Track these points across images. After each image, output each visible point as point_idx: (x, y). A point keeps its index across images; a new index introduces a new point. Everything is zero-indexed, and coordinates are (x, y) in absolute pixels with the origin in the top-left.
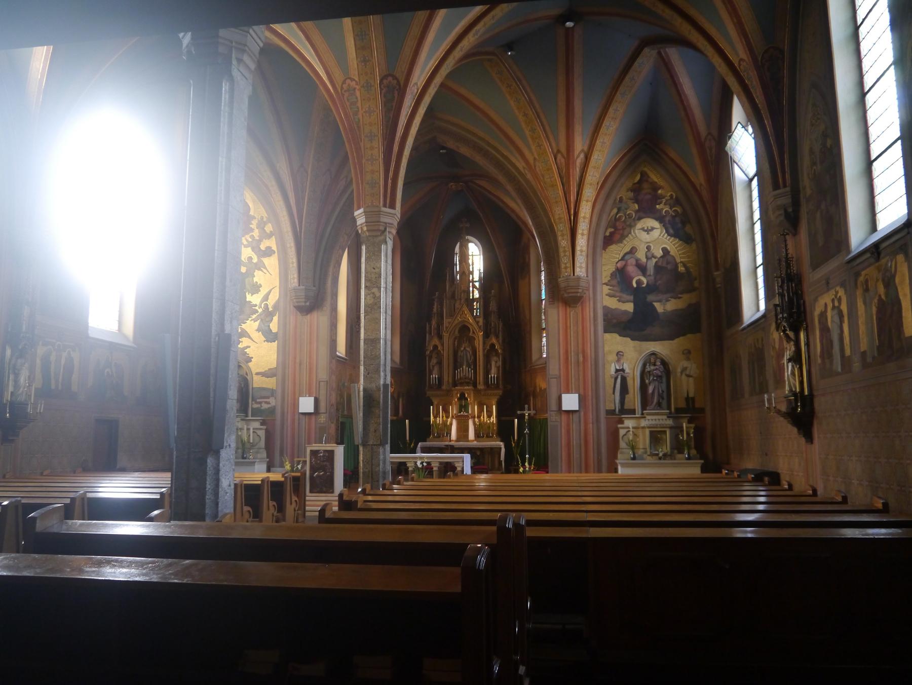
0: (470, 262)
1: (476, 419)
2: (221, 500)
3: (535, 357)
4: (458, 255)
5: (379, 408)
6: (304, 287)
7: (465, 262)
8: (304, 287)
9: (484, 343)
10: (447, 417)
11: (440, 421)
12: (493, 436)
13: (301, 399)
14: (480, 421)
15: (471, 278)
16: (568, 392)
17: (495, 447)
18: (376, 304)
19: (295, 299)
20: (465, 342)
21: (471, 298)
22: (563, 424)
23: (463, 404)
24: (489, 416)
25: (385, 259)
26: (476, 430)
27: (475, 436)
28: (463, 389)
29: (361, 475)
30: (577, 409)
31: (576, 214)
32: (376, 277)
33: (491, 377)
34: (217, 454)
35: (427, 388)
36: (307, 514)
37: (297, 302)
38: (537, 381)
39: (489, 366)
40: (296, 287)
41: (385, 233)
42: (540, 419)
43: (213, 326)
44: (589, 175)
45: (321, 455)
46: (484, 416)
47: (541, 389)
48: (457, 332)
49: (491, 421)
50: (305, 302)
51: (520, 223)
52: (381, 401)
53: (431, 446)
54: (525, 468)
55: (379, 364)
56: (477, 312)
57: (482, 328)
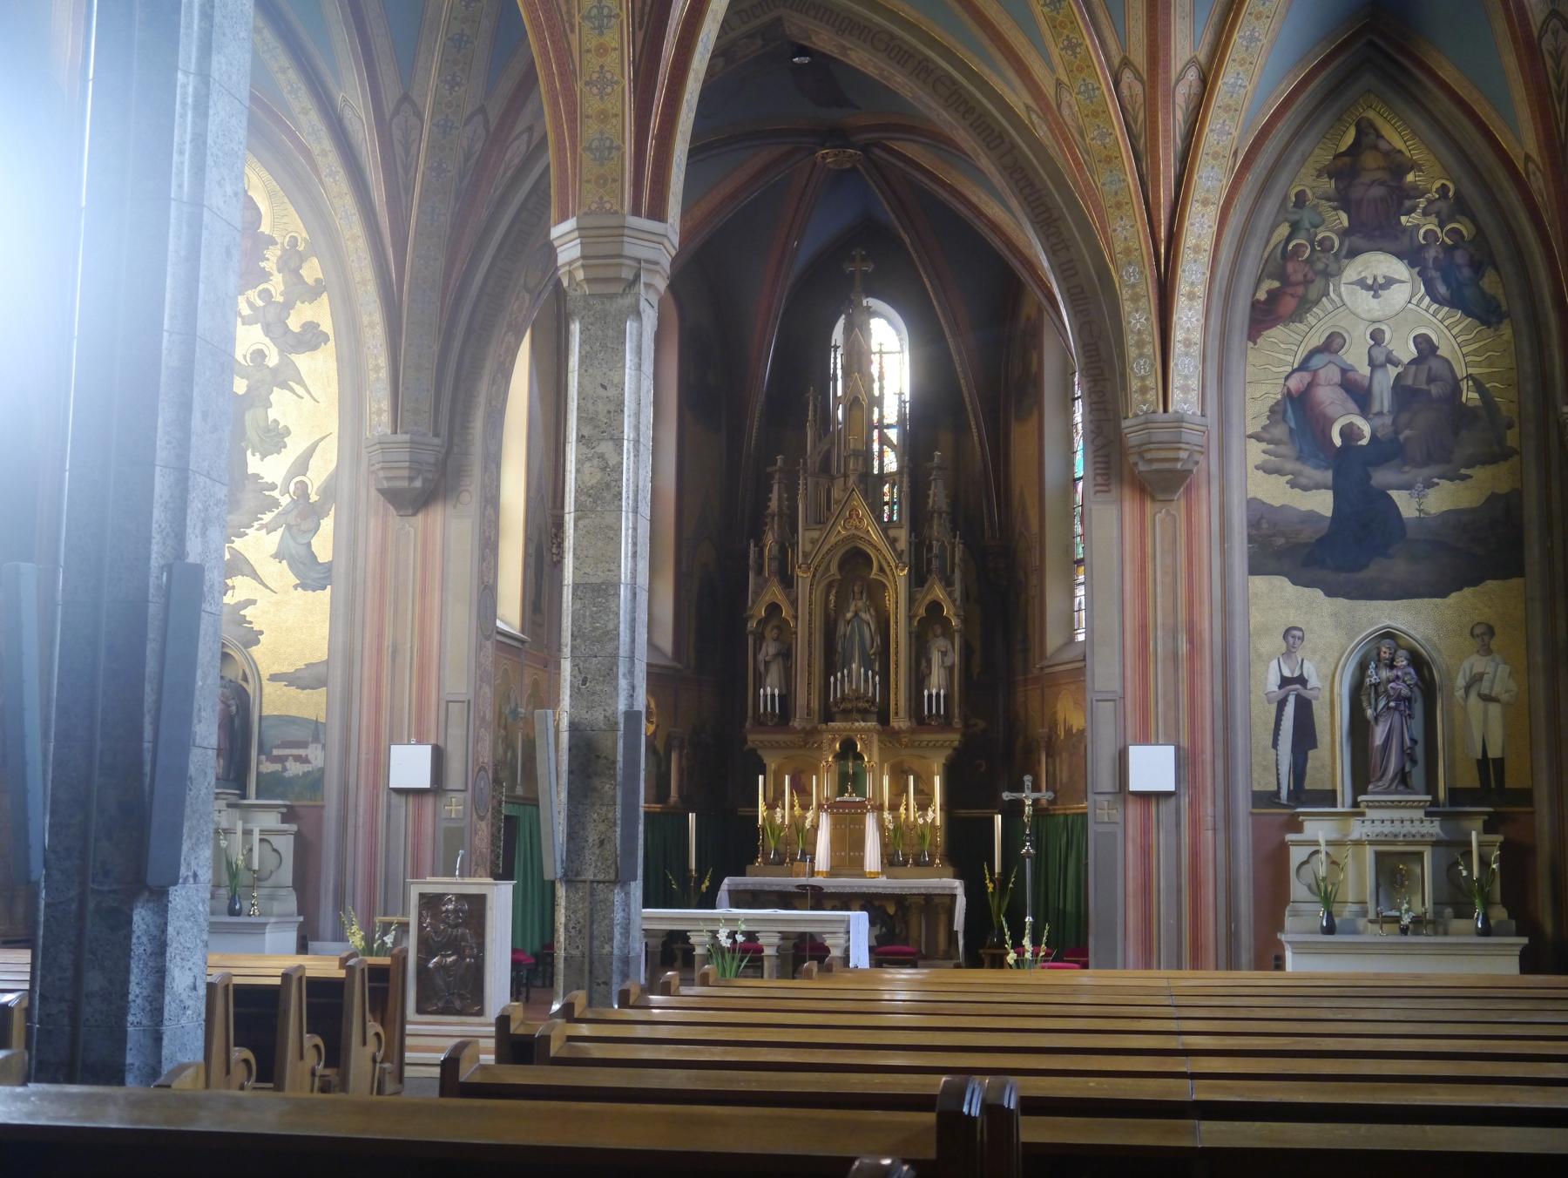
0: (875, 370)
2: (168, 1029)
3: (1053, 640)
4: (840, 352)
5: (614, 777)
6: (407, 437)
8: (407, 437)
9: (911, 600)
10: (805, 807)
11: (783, 817)
12: (930, 864)
13: (396, 750)
14: (896, 818)
15: (876, 417)
16: (1145, 739)
18: (608, 486)
19: (382, 468)
20: (857, 596)
22: (1130, 831)
23: (851, 772)
24: (923, 806)
25: (637, 360)
26: (884, 845)
28: (851, 730)
29: (560, 965)
30: (1170, 786)
31: (1173, 238)
32: (609, 412)
33: (930, 696)
34: (160, 897)
35: (748, 725)
36: (409, 1072)
37: (388, 479)
39: (924, 664)
40: (386, 435)
42: (1066, 815)
43: (154, 541)
44: (1212, 131)
45: (450, 907)
46: (907, 805)
47: (1068, 731)
48: (834, 568)
49: (929, 821)
50: (411, 479)
51: (1015, 264)
52: (620, 758)
53: (758, 888)
54: (1021, 953)
57: (905, 558)
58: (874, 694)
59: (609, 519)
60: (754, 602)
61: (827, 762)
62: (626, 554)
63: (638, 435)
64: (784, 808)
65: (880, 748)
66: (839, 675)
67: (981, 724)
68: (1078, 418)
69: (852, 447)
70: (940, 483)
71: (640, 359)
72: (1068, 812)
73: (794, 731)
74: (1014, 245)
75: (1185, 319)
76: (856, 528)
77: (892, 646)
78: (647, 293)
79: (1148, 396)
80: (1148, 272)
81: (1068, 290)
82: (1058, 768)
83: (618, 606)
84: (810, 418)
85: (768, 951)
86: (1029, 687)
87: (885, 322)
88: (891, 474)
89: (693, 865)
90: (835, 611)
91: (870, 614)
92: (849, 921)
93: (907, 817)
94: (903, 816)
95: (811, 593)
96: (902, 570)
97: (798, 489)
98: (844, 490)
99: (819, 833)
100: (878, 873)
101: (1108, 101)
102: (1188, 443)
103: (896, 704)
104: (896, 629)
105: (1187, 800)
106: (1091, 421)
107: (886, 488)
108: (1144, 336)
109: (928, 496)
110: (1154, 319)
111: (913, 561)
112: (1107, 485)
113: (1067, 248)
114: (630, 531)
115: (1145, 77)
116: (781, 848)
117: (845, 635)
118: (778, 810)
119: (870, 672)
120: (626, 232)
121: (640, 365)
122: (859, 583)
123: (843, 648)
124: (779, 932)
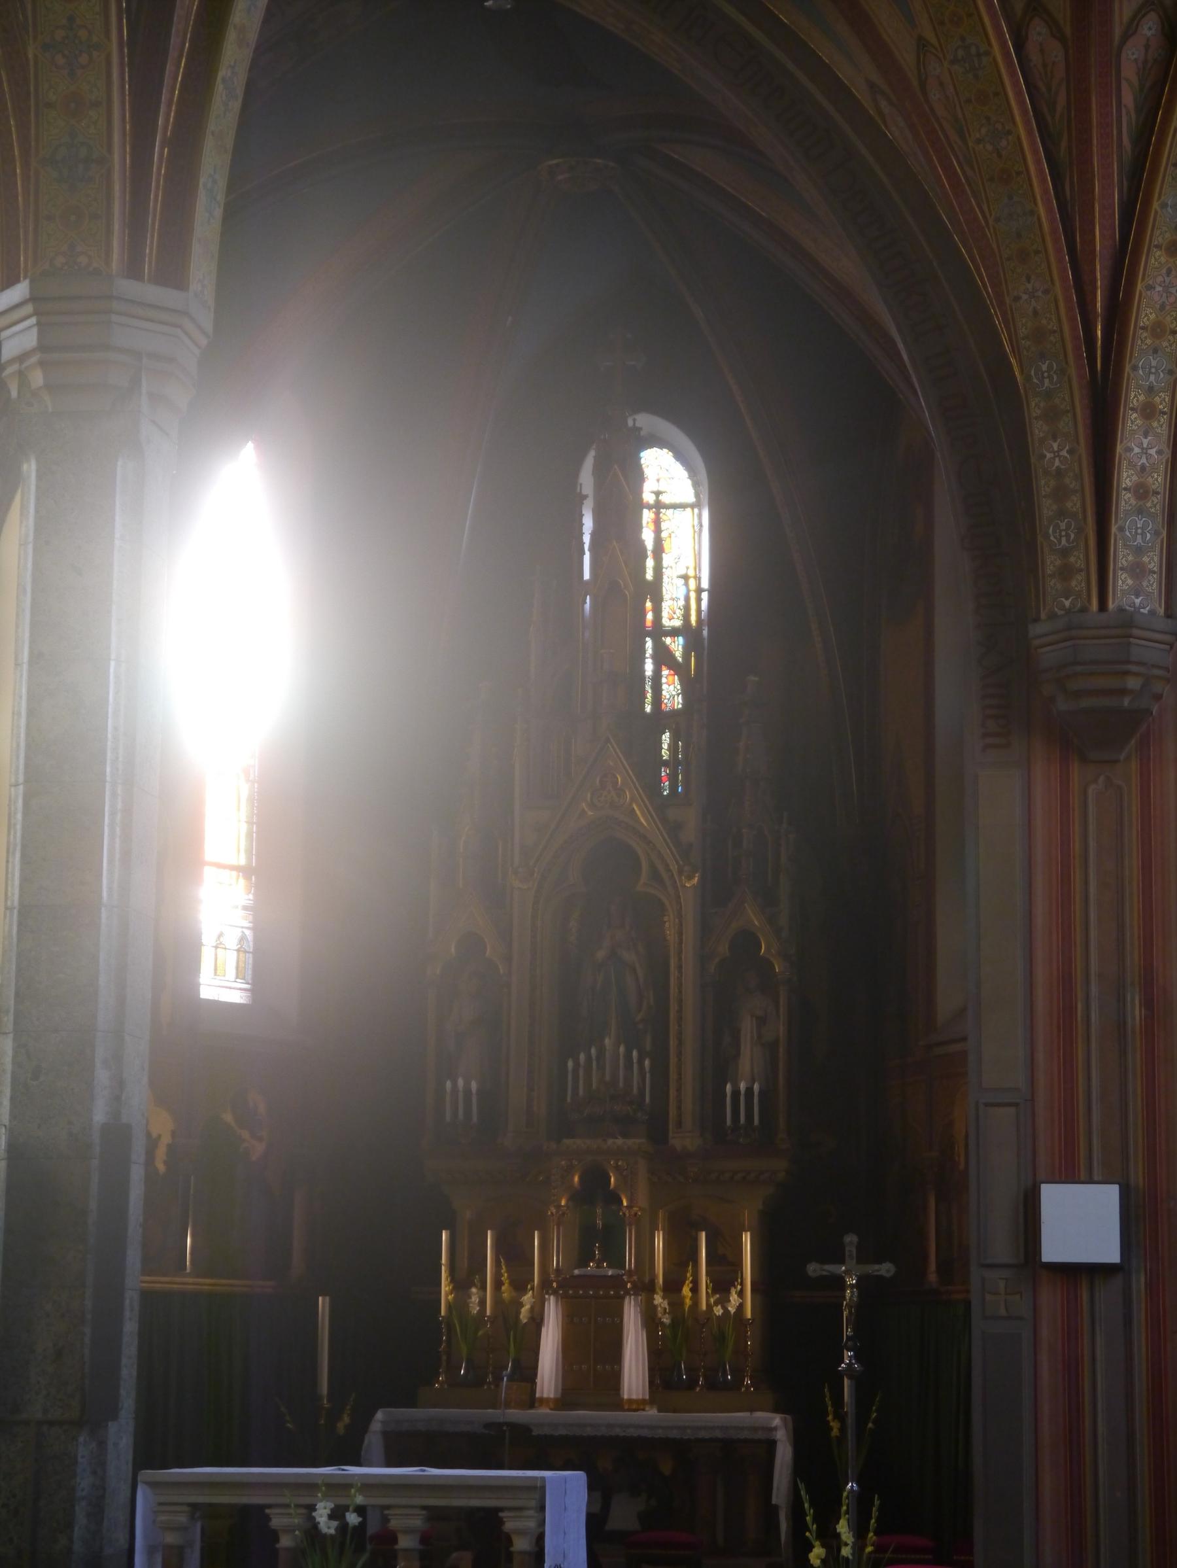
0: (648, 536)
1: (658, 1299)
10: (520, 1286)
11: (482, 1303)
12: (738, 1383)
14: (676, 1306)
16: (1069, 1174)
17: (745, 1435)
22: (1045, 1333)
24: (723, 1284)
27: (651, 1383)
30: (1111, 1253)
33: (736, 1093)
49: (732, 1310)
61: (559, 1207)
64: (484, 1288)
66: (582, 1057)
75: (1137, 450)
79: (1074, 583)
80: (1073, 371)
85: (405, 1542)
88: (674, 713)
92: (543, 1488)
94: (688, 1302)
96: (690, 878)
99: (544, 1330)
100: (643, 1401)
101: (1003, 71)
102: (1139, 663)
103: (679, 1108)
105: (1143, 1279)
108: (1067, 481)
110: (1083, 450)
115: (1068, 30)
118: (474, 1290)
119: (635, 1053)
124: (424, 1508)
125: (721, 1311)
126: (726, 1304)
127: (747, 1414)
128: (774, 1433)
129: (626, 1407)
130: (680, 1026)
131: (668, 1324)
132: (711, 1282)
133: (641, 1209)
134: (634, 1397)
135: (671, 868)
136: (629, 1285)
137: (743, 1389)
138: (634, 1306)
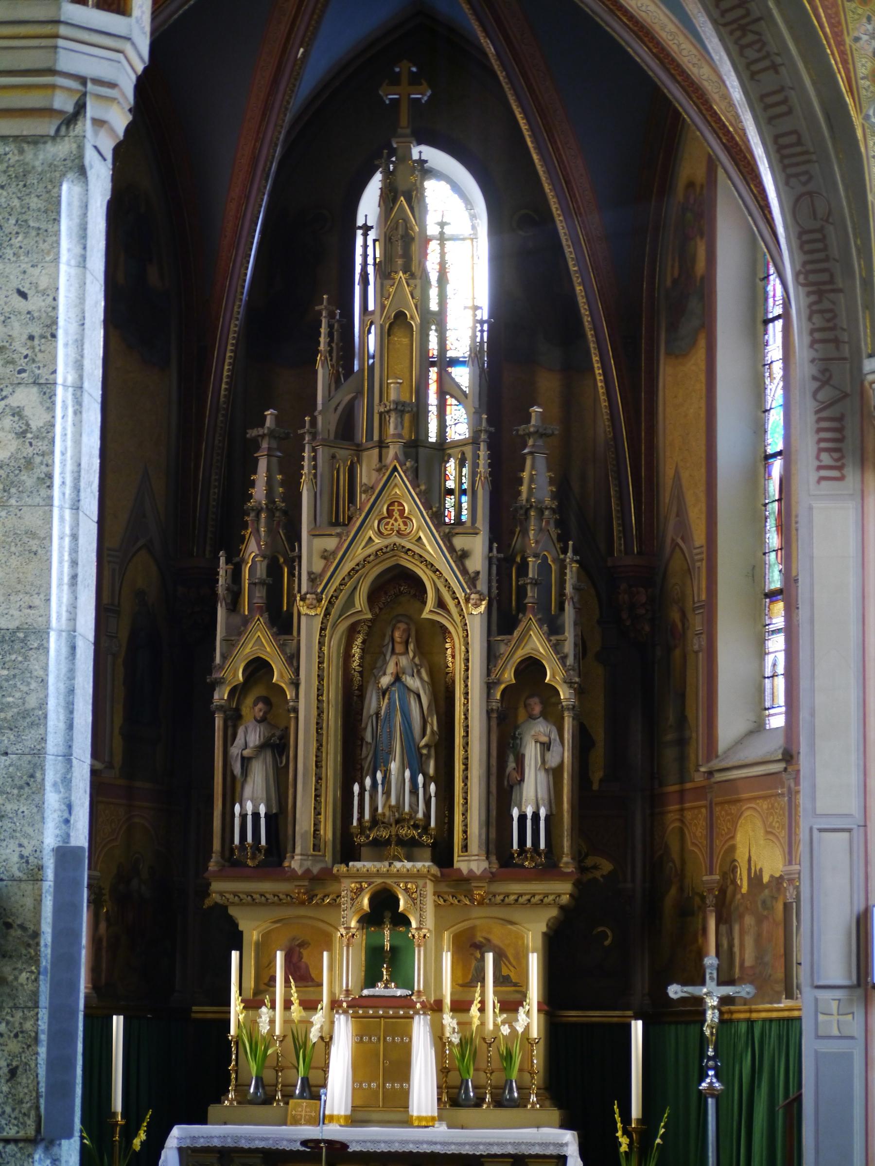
4: (372, 235)
5: (35, 960)
7: (407, 269)
9: (491, 656)
10: (310, 1006)
11: (272, 1022)
18: (29, 463)
20: (399, 648)
21: (433, 438)
23: (387, 946)
25: (78, 250)
26: (443, 1071)
28: (388, 875)
32: (31, 338)
33: (522, 818)
35: (212, 866)
38: (741, 839)
39: (511, 765)
41: (78, 128)
42: (751, 1023)
46: (482, 1002)
47: (756, 880)
48: (360, 602)
49: (520, 1029)
51: (675, 92)
53: (230, 1143)
55: (38, 753)
56: (459, 507)
57: (482, 585)
58: (427, 815)
59: (31, 519)
60: (224, 657)
61: (348, 928)
62: (60, 579)
63: (81, 377)
64: (273, 1007)
65: (437, 906)
66: (368, 781)
67: (607, 866)
68: (775, 351)
69: (393, 396)
70: (541, 459)
71: (85, 248)
72: (754, 1016)
73: (292, 876)
74: (673, 60)
76: (399, 532)
77: (459, 732)
78: (96, 134)
81: (776, 138)
82: (736, 942)
83: (45, 668)
84: (322, 347)
86: (687, 805)
87: (448, 187)
89: (118, 1105)
90: (361, 673)
91: (421, 679)
93: (483, 1024)
94: (476, 1022)
95: (321, 644)
96: (476, 605)
97: (302, 467)
98: (379, 470)
100: (433, 1119)
103: (465, 832)
104: (466, 705)
106: (812, 361)
107: (451, 467)
109: (520, 481)
111: (495, 591)
112: (840, 468)
113: (775, 67)
114: (67, 540)
116: (269, 1076)
117: (377, 714)
118: (264, 1010)
119: (420, 778)
120: (63, 30)
121: (84, 258)
122: (402, 626)
123: (374, 735)
125: (509, 1030)
126: (514, 1024)
127: (534, 1130)
128: (565, 1149)
129: (416, 1123)
130: (466, 751)
131: (456, 1043)
132: (498, 1002)
133: (429, 931)
134: (424, 1114)
135: (458, 596)
136: (418, 1006)
137: (529, 1106)
138: (424, 1026)
